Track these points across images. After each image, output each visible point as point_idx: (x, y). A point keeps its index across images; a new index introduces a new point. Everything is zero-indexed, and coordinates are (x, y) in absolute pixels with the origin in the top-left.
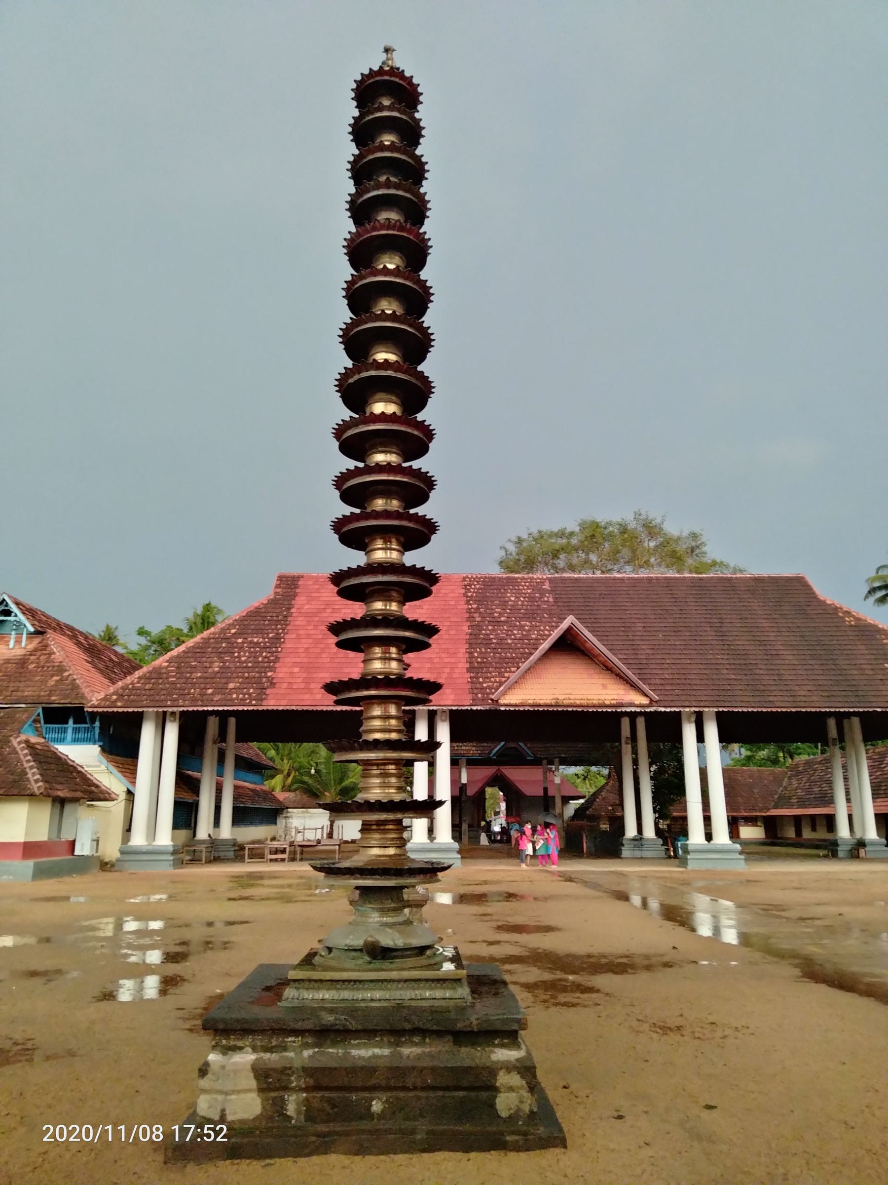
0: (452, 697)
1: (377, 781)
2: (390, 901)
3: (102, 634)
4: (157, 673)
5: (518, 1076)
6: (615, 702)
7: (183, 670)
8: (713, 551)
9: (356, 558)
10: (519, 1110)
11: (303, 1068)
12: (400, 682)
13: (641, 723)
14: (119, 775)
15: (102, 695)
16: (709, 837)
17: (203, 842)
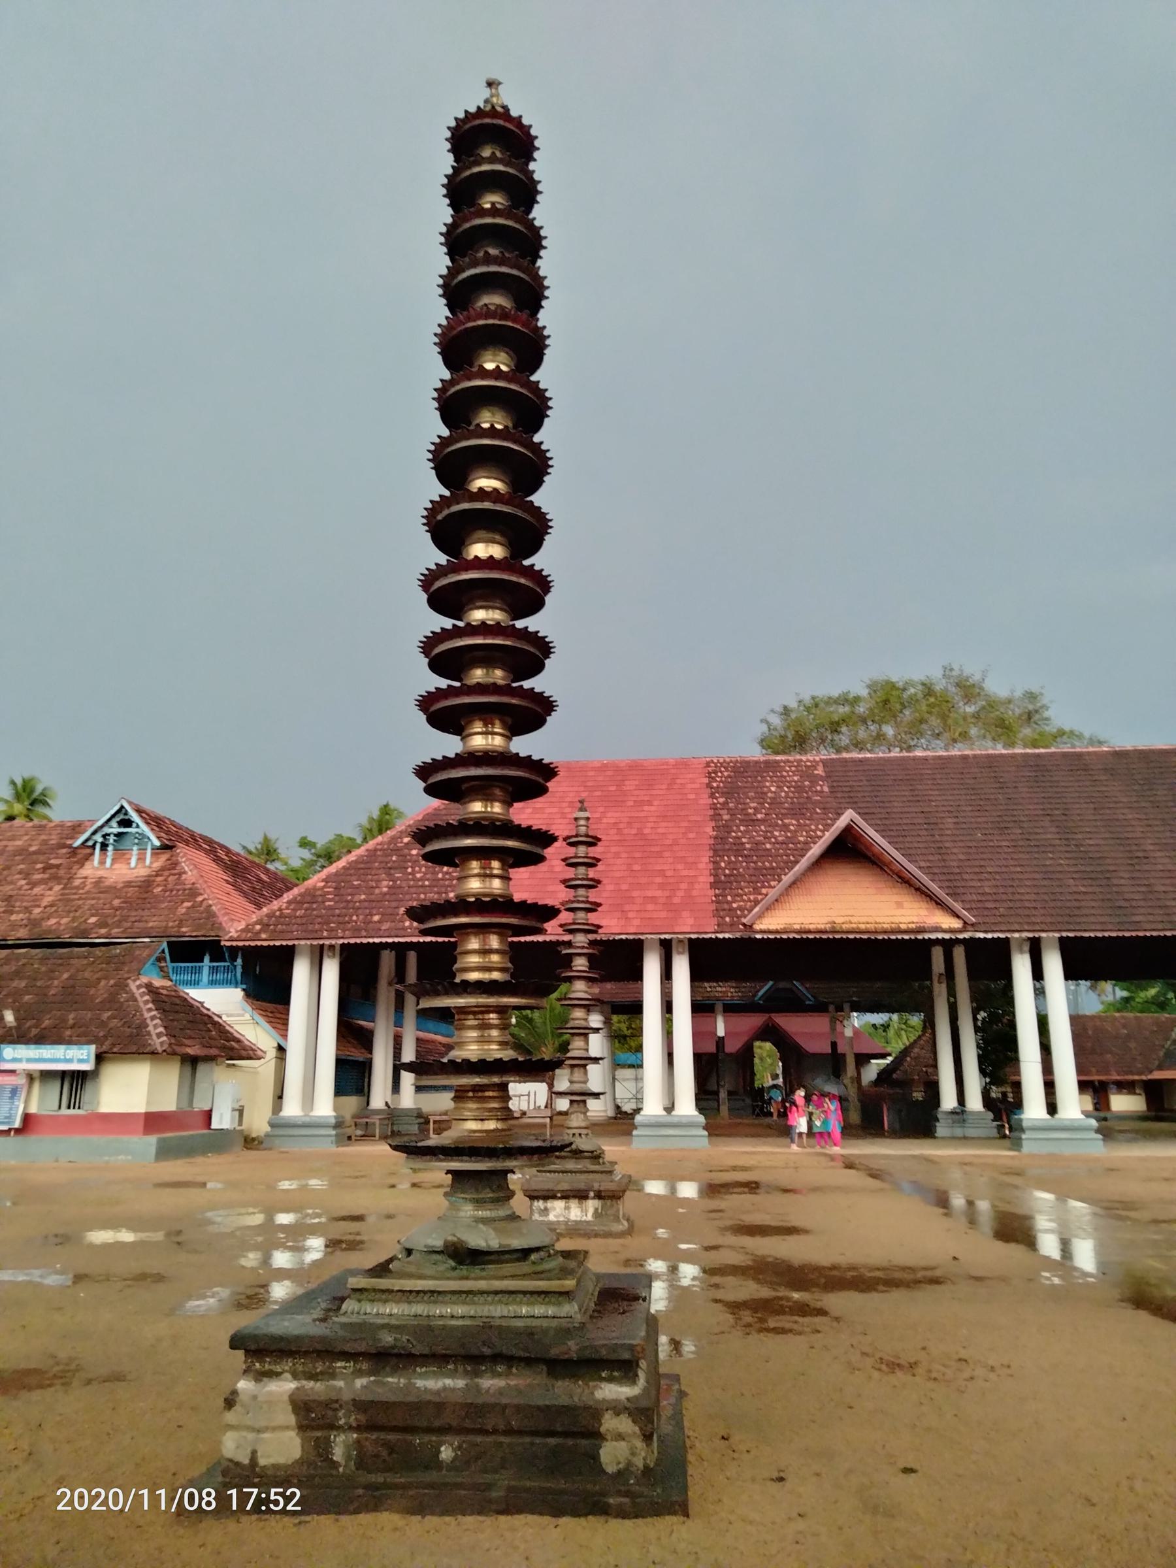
0: (691, 921)
1: (474, 1034)
2: (488, 1190)
3: (259, 846)
4: (311, 897)
5: (630, 1421)
6: (914, 926)
7: (342, 891)
8: (1060, 716)
9: (448, 745)
10: (629, 1464)
11: (354, 1400)
12: (502, 904)
13: (959, 954)
14: (267, 1026)
15: (242, 926)
16: (1052, 1108)
17: (377, 1112)
